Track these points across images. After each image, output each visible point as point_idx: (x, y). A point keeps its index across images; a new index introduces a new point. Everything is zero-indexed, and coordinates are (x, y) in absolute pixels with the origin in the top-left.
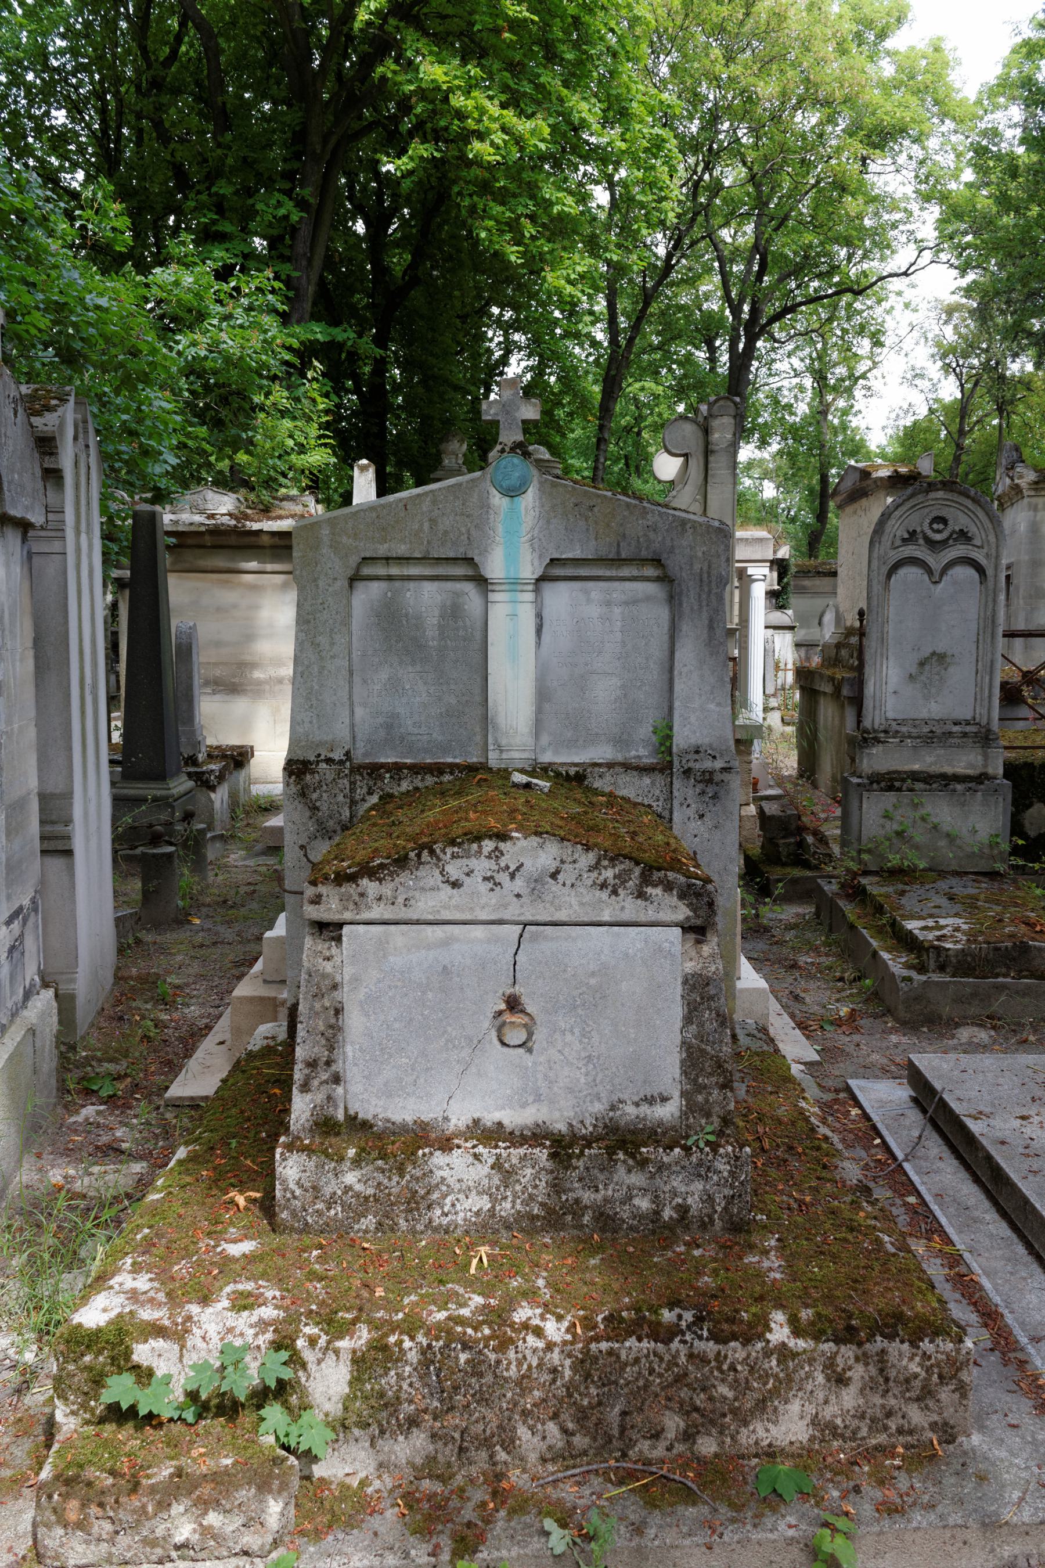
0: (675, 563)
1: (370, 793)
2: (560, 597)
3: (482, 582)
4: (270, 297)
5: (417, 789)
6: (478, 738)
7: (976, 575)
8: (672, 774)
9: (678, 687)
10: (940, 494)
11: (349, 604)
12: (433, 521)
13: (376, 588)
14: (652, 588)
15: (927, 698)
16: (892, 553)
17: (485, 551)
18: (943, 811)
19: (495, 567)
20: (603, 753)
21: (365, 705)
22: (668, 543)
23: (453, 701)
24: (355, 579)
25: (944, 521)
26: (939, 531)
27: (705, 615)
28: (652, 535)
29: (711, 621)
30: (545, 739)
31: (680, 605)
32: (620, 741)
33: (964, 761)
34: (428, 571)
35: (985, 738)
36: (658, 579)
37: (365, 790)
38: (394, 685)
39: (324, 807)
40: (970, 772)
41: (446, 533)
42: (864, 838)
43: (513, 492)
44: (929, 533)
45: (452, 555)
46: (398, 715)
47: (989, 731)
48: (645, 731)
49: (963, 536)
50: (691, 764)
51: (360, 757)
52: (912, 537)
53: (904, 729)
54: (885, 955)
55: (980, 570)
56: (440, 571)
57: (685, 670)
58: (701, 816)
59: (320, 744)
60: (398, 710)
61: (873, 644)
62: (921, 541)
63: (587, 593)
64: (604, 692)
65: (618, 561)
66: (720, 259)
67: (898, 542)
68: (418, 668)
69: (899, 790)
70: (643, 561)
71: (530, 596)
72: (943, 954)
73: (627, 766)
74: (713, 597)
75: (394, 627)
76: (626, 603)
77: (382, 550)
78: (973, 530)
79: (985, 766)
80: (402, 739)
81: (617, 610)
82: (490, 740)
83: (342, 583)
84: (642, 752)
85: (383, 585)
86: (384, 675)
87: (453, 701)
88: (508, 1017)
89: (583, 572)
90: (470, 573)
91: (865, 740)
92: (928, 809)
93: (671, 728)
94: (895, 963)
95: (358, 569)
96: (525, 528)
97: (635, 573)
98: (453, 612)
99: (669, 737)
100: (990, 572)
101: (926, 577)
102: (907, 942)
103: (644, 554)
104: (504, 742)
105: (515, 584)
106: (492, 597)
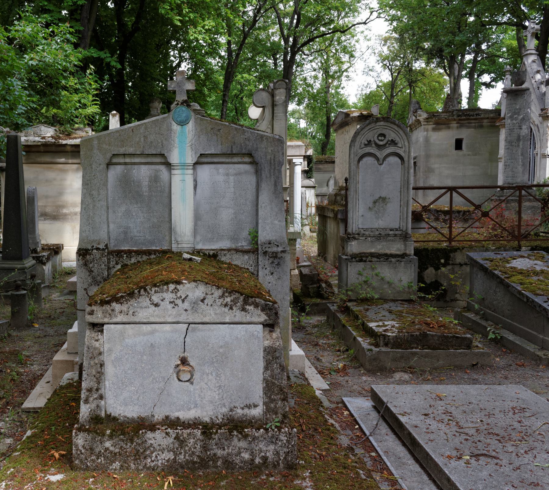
0: (259, 156)
1: (117, 264)
2: (205, 172)
3: (168, 165)
4: (68, 35)
5: (139, 262)
6: (167, 238)
7: (399, 161)
9: (261, 213)
12: (145, 137)
13: (119, 168)
14: (247, 167)
15: (377, 218)
16: (360, 151)
17: (170, 151)
18: (386, 271)
19: (175, 158)
22: (255, 146)
23: (155, 220)
24: (109, 164)
26: (381, 140)
27: (272, 179)
28: (247, 142)
30: (198, 238)
31: (261, 175)
32: (234, 239)
33: (395, 248)
35: (405, 237)
36: (250, 163)
37: (114, 263)
39: (96, 271)
41: (151, 142)
42: (349, 284)
43: (182, 123)
44: (377, 141)
45: (154, 153)
47: (407, 233)
50: (267, 249)
51: (112, 247)
52: (369, 143)
53: (367, 233)
55: (401, 158)
57: (264, 205)
58: (272, 274)
60: (130, 225)
61: (352, 193)
62: (373, 145)
63: (217, 170)
64: (226, 216)
65: (232, 155)
67: (363, 146)
68: (139, 205)
69: (365, 261)
70: (244, 155)
71: (191, 172)
72: (387, 339)
73: (237, 250)
74: (276, 171)
76: (236, 174)
77: (122, 151)
78: (397, 139)
79: (405, 250)
80: (132, 238)
81: (232, 178)
82: (173, 239)
84: (244, 244)
85: (122, 167)
88: (182, 368)
89: (216, 160)
93: (257, 232)
94: (364, 343)
96: (188, 140)
97: (240, 160)
98: (155, 179)
99: (257, 237)
100: (406, 159)
101: (376, 162)
102: (370, 333)
103: (244, 151)
104: (179, 239)
105: (184, 166)
106: (173, 172)
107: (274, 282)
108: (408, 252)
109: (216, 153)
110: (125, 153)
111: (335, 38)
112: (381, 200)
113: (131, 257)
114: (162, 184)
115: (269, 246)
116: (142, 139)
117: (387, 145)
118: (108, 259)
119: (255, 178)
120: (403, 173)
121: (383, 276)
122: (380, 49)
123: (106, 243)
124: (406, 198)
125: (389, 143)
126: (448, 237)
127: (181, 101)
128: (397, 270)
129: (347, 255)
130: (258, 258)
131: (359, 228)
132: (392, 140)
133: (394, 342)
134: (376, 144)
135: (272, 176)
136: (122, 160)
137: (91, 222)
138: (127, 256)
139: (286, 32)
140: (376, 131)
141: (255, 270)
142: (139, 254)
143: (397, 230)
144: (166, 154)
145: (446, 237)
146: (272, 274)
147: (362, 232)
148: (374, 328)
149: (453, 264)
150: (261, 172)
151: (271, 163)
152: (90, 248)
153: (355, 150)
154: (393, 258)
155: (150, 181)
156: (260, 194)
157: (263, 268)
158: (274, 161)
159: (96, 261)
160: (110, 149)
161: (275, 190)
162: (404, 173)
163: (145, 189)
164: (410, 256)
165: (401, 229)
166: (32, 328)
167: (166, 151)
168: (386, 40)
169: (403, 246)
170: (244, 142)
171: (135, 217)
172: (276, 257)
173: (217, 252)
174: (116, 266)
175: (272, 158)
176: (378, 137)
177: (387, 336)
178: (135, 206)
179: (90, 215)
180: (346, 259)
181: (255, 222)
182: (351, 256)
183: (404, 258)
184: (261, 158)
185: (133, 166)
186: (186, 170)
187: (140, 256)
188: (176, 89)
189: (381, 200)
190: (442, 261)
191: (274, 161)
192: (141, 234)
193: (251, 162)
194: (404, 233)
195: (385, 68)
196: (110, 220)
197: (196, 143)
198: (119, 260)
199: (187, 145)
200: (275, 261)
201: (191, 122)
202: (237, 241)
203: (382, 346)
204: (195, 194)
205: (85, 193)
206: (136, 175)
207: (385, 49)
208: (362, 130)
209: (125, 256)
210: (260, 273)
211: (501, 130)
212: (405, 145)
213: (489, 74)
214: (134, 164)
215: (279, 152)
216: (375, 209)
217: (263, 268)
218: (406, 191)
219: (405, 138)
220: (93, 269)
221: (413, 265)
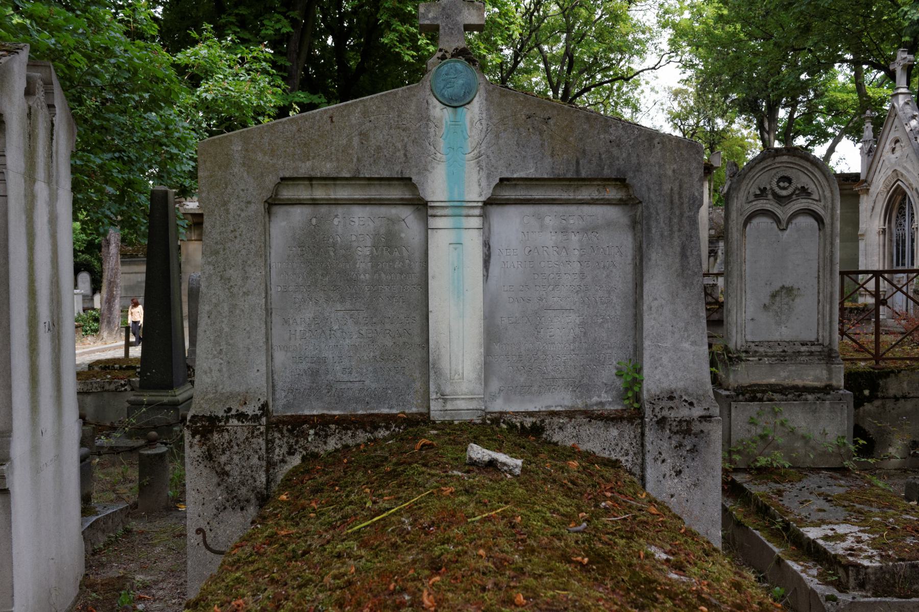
0: (641, 183)
1: (291, 453)
2: (511, 224)
3: (421, 206)
4: (264, 63)
5: (346, 447)
6: (418, 385)
7: (816, 224)
8: (643, 425)
9: (648, 323)
10: (785, 158)
11: (266, 232)
12: (364, 135)
13: (298, 214)
14: (612, 213)
15: (778, 324)
16: (747, 206)
17: (424, 170)
18: (798, 418)
19: (437, 187)
20: (560, 400)
22: (634, 160)
23: (389, 343)
24: (272, 203)
25: (788, 180)
26: (784, 188)
27: (677, 242)
28: (615, 151)
29: (684, 248)
30: (495, 385)
31: (649, 230)
32: (580, 386)
33: (812, 375)
34: (358, 194)
35: (828, 356)
36: (620, 203)
37: (285, 449)
39: (235, 473)
40: (816, 384)
41: (379, 148)
42: (733, 441)
43: (456, 103)
44: (777, 190)
45: (385, 174)
47: (831, 350)
48: (607, 373)
49: (804, 192)
50: (665, 413)
51: (279, 409)
52: (762, 193)
53: (761, 350)
54: (790, 563)
55: (819, 219)
56: (373, 193)
57: (655, 304)
58: (679, 473)
59: (231, 396)
60: (325, 354)
61: (735, 280)
62: (770, 197)
63: (540, 218)
64: (561, 330)
65: (578, 181)
66: (545, 63)
67: (752, 198)
68: (348, 305)
69: (761, 400)
70: (605, 181)
71: (476, 222)
72: (862, 573)
73: (591, 416)
74: (685, 221)
75: (320, 259)
76: (585, 230)
77: (304, 169)
78: (811, 187)
79: (830, 379)
80: (329, 387)
81: (574, 238)
82: (432, 388)
83: (257, 208)
84: (605, 397)
85: (307, 210)
87: (389, 343)
89: (537, 194)
91: (730, 359)
92: (785, 416)
93: (639, 370)
94: (809, 575)
96: (469, 145)
97: (595, 195)
98: (388, 241)
99: (637, 382)
100: (827, 220)
101: (775, 225)
102: (812, 552)
103: (607, 172)
104: (448, 390)
105: (459, 208)
106: (433, 223)
107: (684, 495)
108: (834, 383)
109: (538, 176)
110: (313, 174)
111: (615, 87)
112: (784, 291)
113: (326, 436)
114: (405, 253)
115: (671, 404)
116: (356, 141)
117: (794, 197)
118: (267, 442)
119: (630, 239)
120: (822, 245)
121: (792, 425)
122: (669, 105)
123: (262, 401)
124: (829, 287)
125: (797, 192)
126: (873, 352)
127: (451, 51)
128: (817, 414)
129: (727, 389)
130: (643, 434)
131: (747, 342)
132: (803, 187)
133: (877, 579)
134: (775, 195)
135: (676, 234)
136: (304, 193)
137: (224, 347)
138: (316, 434)
139: (555, 80)
140: (774, 172)
141: (634, 464)
142: (346, 429)
143: (813, 344)
144: (415, 179)
145: (869, 353)
146: (679, 473)
147: (753, 348)
148: (821, 542)
149: (883, 398)
150: (648, 224)
151: (672, 202)
152: (221, 414)
153: (739, 205)
154: (810, 393)
155: (375, 246)
156: (646, 276)
157: (656, 460)
158: (680, 197)
159: (236, 448)
160: (273, 165)
161: (682, 266)
162: (825, 244)
163: (363, 265)
164: (839, 389)
165: (820, 342)
166: (175, 513)
167: (415, 170)
168: (676, 93)
169: (824, 372)
170: (608, 151)
171: (338, 334)
172: (688, 432)
173: (543, 421)
174: (288, 458)
175: (676, 189)
176: (778, 182)
177: (864, 567)
178: (339, 306)
179: (221, 330)
180: (727, 396)
181: (630, 344)
182: (735, 390)
183: (829, 394)
184: (649, 189)
185: (333, 208)
186: (464, 219)
187: (350, 433)
188: (439, 22)
189: (784, 291)
190: (867, 392)
191: (680, 197)
192: (355, 377)
193: (621, 200)
194: (826, 349)
195: (675, 128)
196: (275, 341)
197: (489, 153)
198: (297, 442)
199: (469, 156)
200: (685, 442)
201: (476, 99)
202: (588, 391)
203: (854, 589)
204: (486, 277)
205: (210, 276)
206: (340, 231)
207: (675, 104)
208: (750, 171)
209: (312, 432)
210: (650, 474)
211: (861, 196)
212: (825, 196)
213: (804, 136)
214: (337, 203)
215: (691, 175)
216: (775, 307)
217: (656, 460)
218: (828, 276)
219: (826, 184)
220: (227, 468)
221: (845, 407)
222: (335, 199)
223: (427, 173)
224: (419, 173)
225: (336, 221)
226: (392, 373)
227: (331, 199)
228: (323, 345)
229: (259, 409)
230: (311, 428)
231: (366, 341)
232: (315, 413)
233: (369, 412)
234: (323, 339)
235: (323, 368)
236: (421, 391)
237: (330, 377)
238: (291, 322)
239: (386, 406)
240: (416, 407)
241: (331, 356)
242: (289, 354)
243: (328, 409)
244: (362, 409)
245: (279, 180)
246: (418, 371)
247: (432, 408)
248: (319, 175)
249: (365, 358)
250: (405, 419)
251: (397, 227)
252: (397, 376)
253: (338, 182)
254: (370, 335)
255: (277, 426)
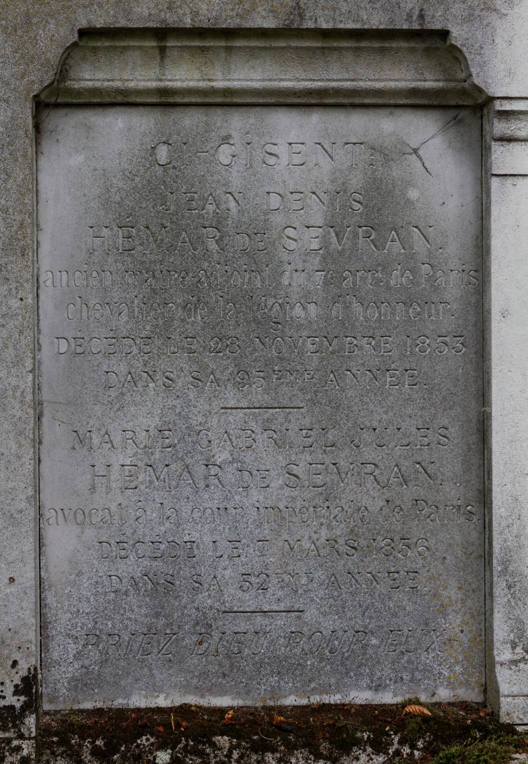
6: (455, 622)
13: (119, 134)
21: (80, 517)
23: (372, 500)
24: (53, 101)
38: (177, 452)
46: (191, 548)
56: (333, 74)
68: (257, 393)
75: (180, 265)
80: (204, 628)
82: (501, 631)
86: (145, 414)
87: (372, 500)
90: (431, 83)
95: (63, 71)
98: (371, 211)
110: (171, 20)
114: (420, 246)
144: (458, 34)
163: (300, 279)
171: (230, 475)
178: (231, 397)
185: (217, 117)
192: (274, 598)
206: (236, 181)
214: (230, 101)
222: (228, 92)
223: (493, 18)
224: (469, 19)
225: (224, 155)
226: (382, 588)
227: (214, 91)
228: (186, 509)
229: (17, 692)
230: (162, 747)
231: (307, 495)
232: (162, 702)
233: (315, 699)
234: (188, 491)
235: (186, 572)
236: (464, 638)
237: (205, 599)
238: (96, 441)
239: (365, 682)
240: (450, 685)
241: (207, 539)
242: (90, 533)
243: (199, 691)
244: (296, 691)
245: (75, 37)
246: (453, 583)
247: (504, 688)
248: (188, 23)
249: (306, 544)
250: (425, 719)
251: (396, 172)
252: (396, 595)
253: (239, 43)
254: (319, 480)
255: (64, 741)
